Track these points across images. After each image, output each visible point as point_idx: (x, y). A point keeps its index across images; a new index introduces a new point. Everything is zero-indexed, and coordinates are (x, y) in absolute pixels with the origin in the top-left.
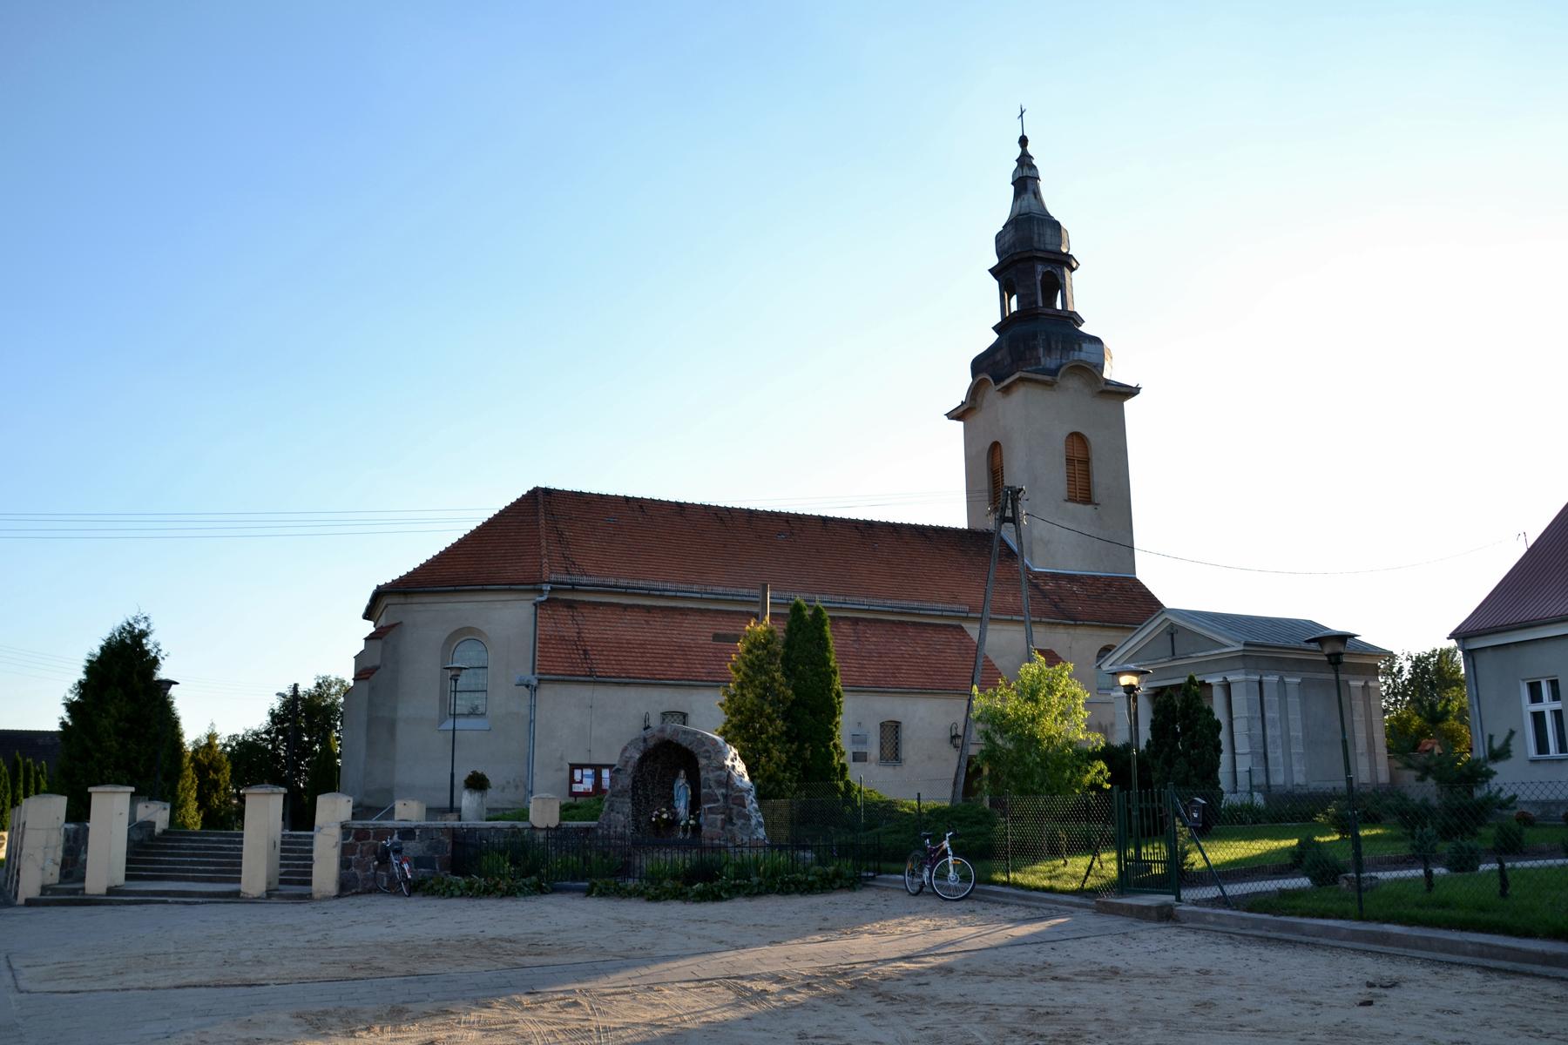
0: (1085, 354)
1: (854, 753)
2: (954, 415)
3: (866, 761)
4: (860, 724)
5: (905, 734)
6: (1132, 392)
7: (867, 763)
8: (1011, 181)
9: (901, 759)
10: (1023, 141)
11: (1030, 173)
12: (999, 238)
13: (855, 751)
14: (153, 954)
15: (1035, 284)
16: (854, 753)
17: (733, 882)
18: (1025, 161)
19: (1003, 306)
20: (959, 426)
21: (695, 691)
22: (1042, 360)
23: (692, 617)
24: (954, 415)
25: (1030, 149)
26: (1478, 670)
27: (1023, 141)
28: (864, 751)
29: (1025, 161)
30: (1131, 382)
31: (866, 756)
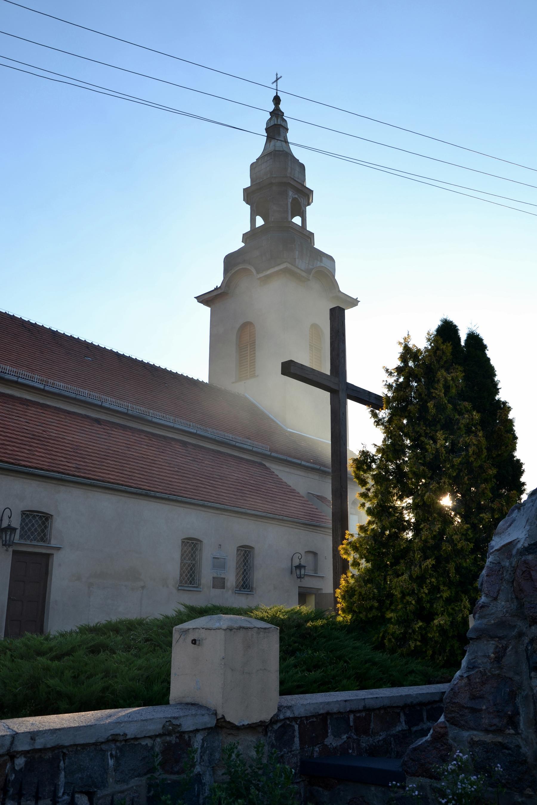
0: (326, 263)
1: (214, 578)
2: (204, 299)
3: (224, 588)
4: (220, 545)
5: (258, 560)
6: (354, 302)
7: (224, 590)
8: (265, 127)
9: (252, 588)
10: (277, 100)
11: (280, 122)
12: (253, 166)
13: (215, 575)
14: (299, 232)
15: (287, 204)
16: (214, 578)
17: (398, 784)
18: (277, 113)
19: (253, 221)
20: (206, 311)
21: (62, 488)
22: (297, 260)
23: (33, 409)
24: (204, 299)
25: (282, 107)
26: (290, 564)
27: (277, 100)
28: (222, 576)
29: (277, 113)
30: (353, 295)
31: (224, 583)
